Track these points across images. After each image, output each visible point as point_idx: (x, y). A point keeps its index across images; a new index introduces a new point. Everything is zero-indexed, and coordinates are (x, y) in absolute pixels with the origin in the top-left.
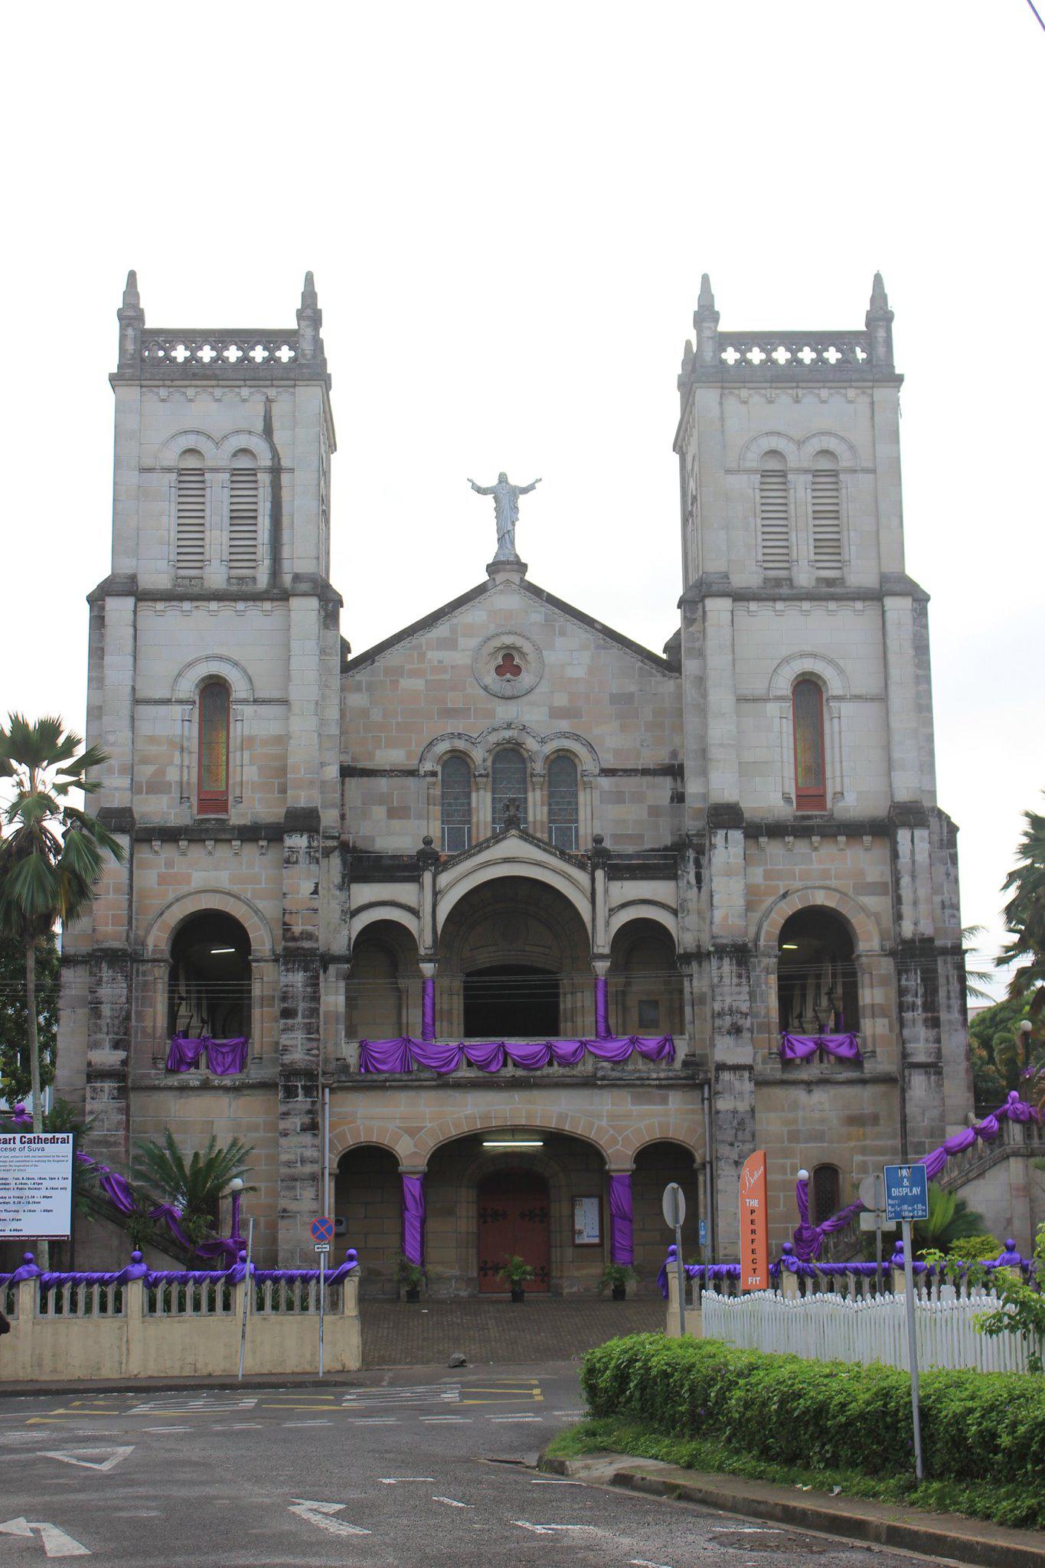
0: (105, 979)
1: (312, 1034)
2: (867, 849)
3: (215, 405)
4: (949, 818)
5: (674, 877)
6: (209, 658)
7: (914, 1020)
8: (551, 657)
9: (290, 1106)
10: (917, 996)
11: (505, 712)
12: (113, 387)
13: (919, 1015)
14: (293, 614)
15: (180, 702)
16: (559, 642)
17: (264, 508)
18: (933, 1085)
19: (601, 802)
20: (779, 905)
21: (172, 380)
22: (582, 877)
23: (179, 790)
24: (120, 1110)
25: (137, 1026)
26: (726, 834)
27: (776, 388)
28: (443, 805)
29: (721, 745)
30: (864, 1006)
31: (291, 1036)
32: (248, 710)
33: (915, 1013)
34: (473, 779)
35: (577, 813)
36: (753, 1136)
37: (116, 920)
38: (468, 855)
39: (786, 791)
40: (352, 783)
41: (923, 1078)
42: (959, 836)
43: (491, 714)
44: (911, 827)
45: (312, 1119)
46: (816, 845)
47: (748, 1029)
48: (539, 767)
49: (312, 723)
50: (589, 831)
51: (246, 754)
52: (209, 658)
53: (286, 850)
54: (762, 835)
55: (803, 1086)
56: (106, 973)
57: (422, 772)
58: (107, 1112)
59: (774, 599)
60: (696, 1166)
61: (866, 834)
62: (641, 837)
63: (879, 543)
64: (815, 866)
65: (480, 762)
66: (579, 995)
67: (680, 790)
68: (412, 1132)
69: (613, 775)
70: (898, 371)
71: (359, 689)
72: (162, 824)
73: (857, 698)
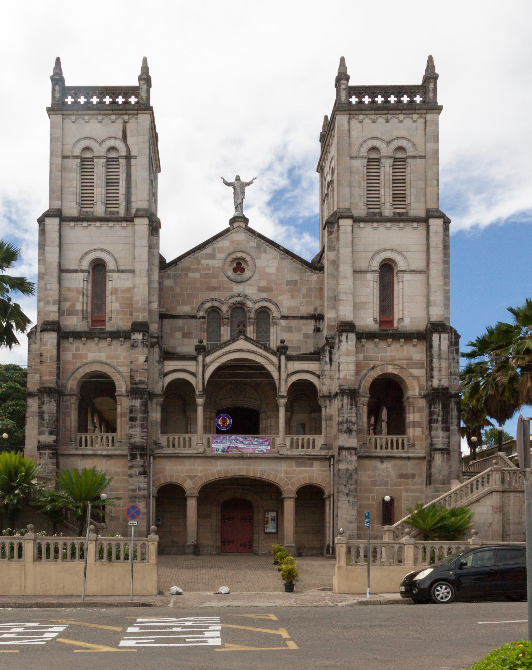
0: (45, 402)
1: (144, 429)
2: (415, 346)
3: (99, 125)
4: (456, 331)
5: (319, 360)
6: (95, 250)
7: (437, 428)
8: (259, 263)
9: (134, 463)
10: (439, 416)
11: (237, 289)
12: (49, 115)
13: (440, 425)
14: (136, 227)
15: (82, 271)
16: (263, 256)
17: (122, 176)
18: (445, 459)
19: (281, 332)
20: (370, 373)
21: (77, 111)
22: (274, 359)
23: (82, 315)
24: (53, 464)
25: (63, 426)
26: (347, 335)
27: (377, 114)
28: (208, 332)
29: (345, 293)
30: (409, 422)
31: (134, 430)
32: (115, 275)
33: (438, 424)
34: (222, 321)
35: (269, 337)
36: (356, 482)
37: (51, 374)
38: (220, 347)
39: (375, 317)
40: (166, 321)
41: (440, 455)
42: (460, 340)
43: (231, 290)
44: (440, 333)
45: (144, 469)
46: (390, 343)
47: (355, 430)
48: (252, 315)
49: (145, 280)
50: (275, 345)
51: (114, 297)
52: (95, 250)
53: (132, 340)
54: (363, 338)
55: (379, 459)
56: (46, 399)
57: (198, 317)
58: (47, 464)
59: (373, 221)
60: (325, 496)
61: (415, 338)
62: (299, 348)
63: (426, 194)
64: (388, 354)
65: (225, 312)
66: (269, 420)
67: (318, 326)
68: (192, 478)
69: (287, 319)
70: (439, 104)
71: (169, 277)
72: (74, 330)
73: (412, 271)
